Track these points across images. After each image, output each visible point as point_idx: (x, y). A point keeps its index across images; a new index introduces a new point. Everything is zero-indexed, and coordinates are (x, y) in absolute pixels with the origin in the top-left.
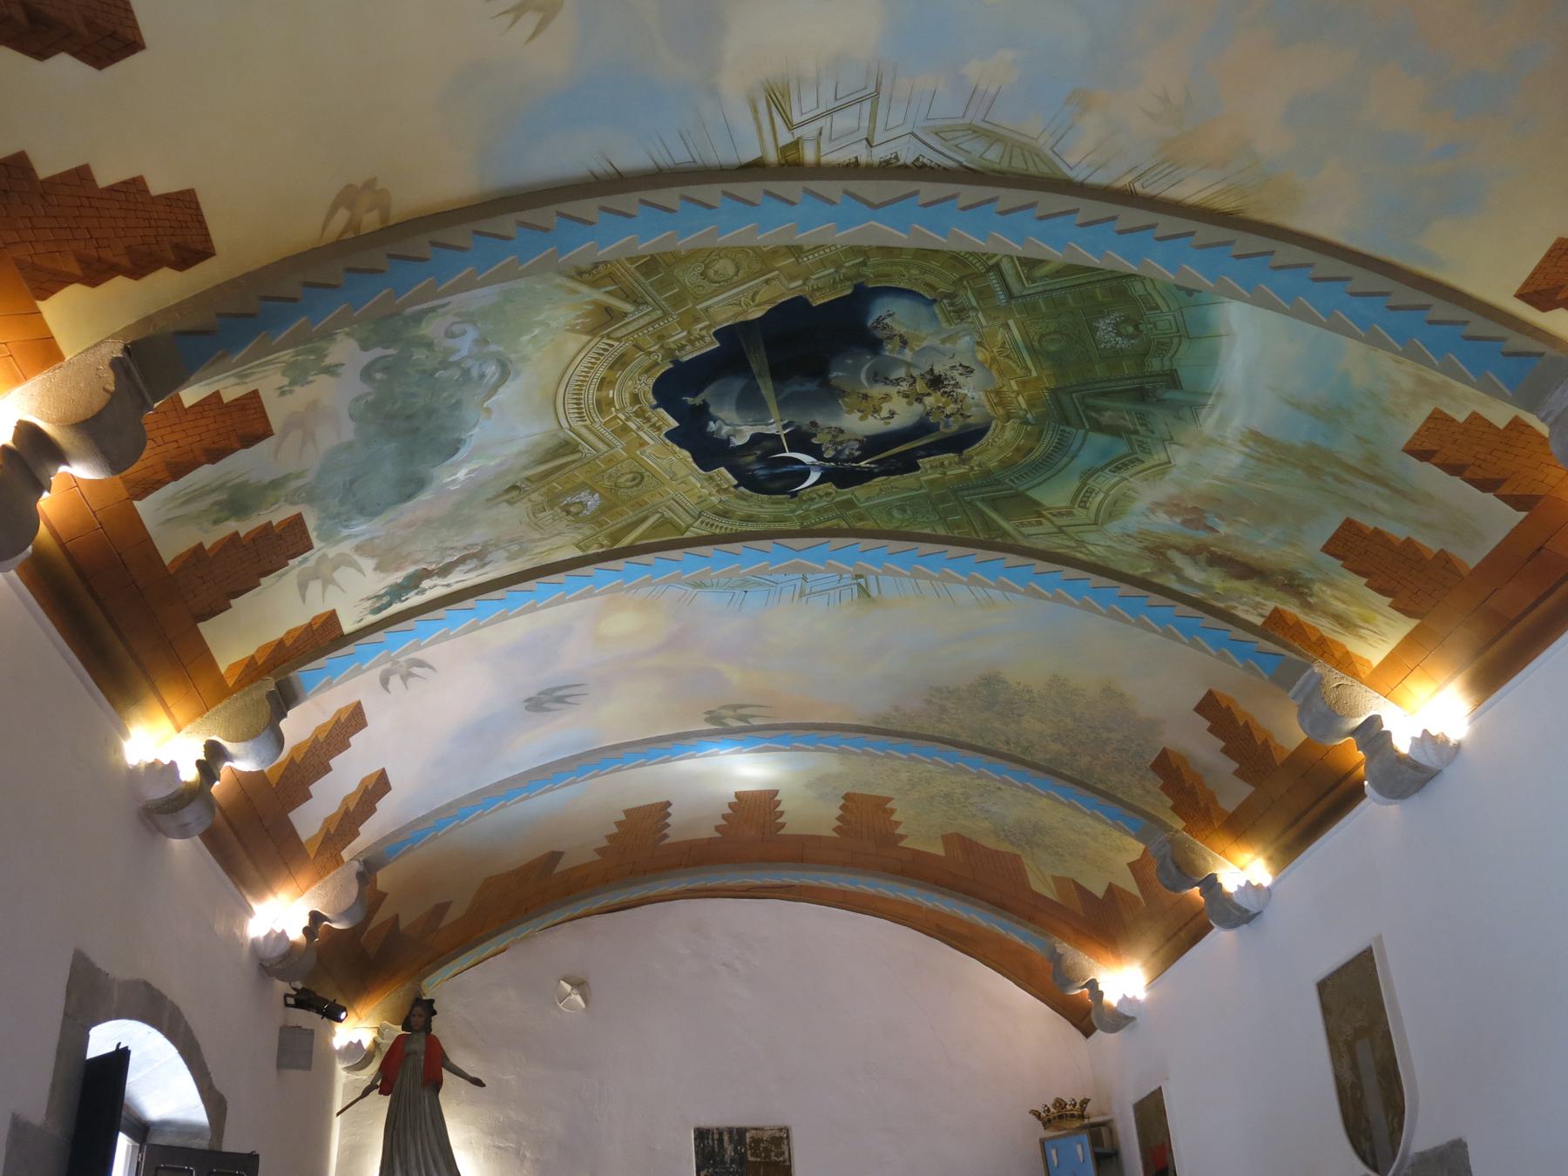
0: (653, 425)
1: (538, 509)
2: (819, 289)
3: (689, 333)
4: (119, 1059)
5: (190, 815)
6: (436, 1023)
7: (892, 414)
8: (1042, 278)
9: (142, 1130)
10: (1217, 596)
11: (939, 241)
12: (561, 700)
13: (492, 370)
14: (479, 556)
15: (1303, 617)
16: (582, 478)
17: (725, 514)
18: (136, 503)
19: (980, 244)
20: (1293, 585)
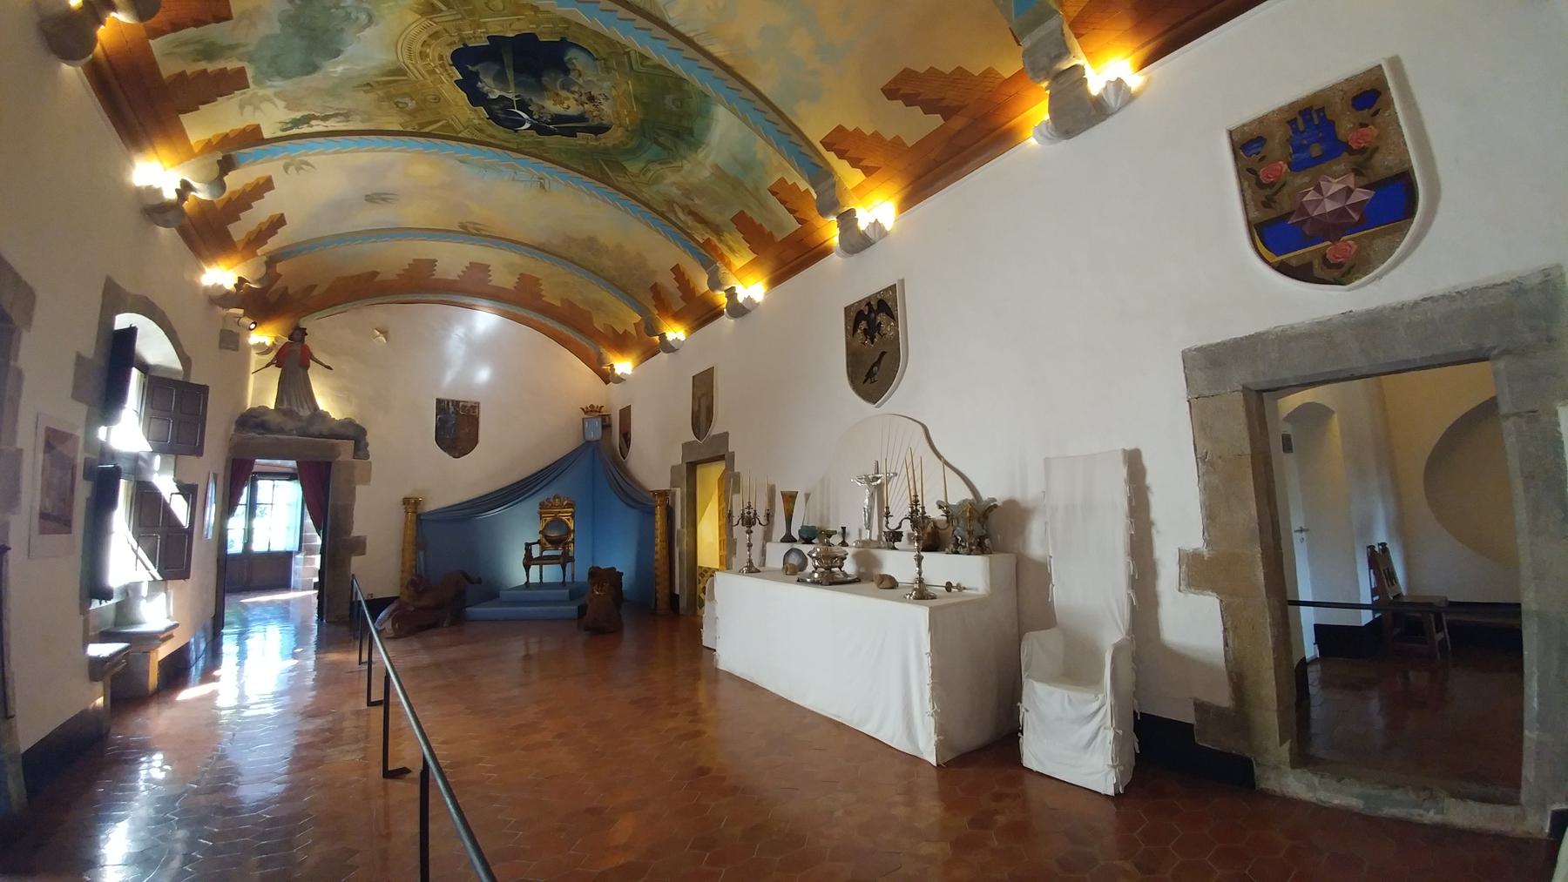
0: (449, 74)
1: (381, 100)
2: (543, 33)
3: (474, 33)
4: (131, 333)
5: (170, 216)
6: (307, 340)
7: (568, 107)
8: (648, 66)
9: (145, 368)
10: (688, 227)
11: (607, 32)
12: (384, 199)
13: (363, 17)
14: (346, 116)
15: (717, 244)
16: (407, 91)
17: (481, 131)
18: (151, 42)
19: (623, 39)
20: (717, 231)
